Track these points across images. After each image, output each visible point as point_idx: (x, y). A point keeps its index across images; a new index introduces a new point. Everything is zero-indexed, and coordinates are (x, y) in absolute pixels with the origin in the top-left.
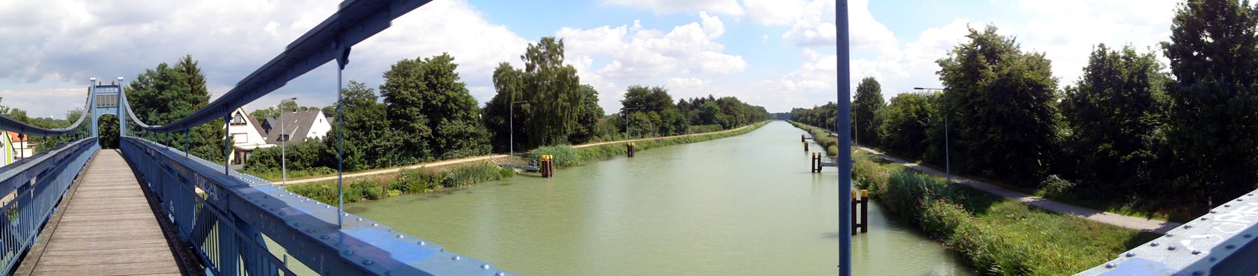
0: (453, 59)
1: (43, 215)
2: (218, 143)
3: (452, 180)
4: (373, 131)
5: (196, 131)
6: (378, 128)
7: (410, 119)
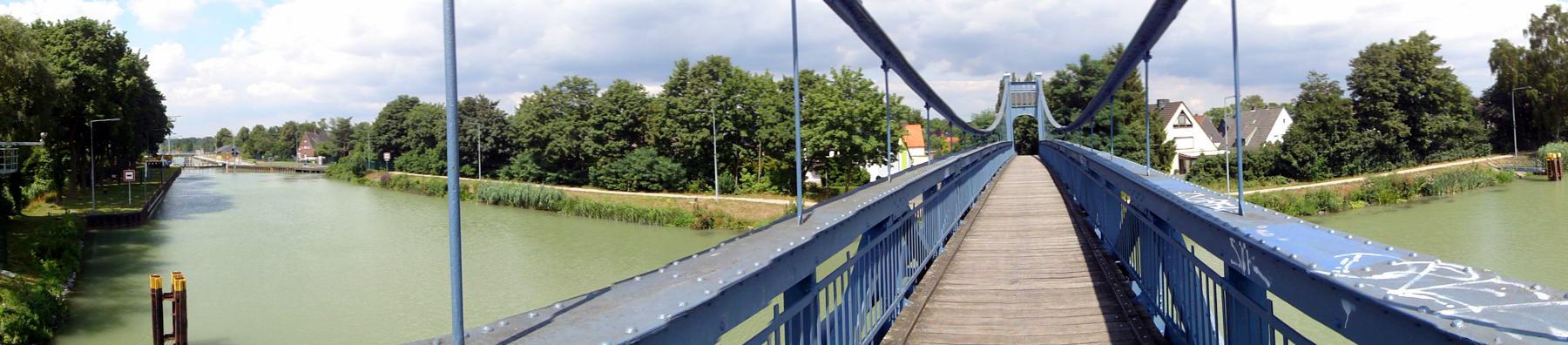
0: (1432, 38)
1: (947, 228)
2: (1156, 148)
3: (1431, 186)
4: (1336, 132)
5: (1129, 134)
6: (1342, 128)
7: (1382, 115)
